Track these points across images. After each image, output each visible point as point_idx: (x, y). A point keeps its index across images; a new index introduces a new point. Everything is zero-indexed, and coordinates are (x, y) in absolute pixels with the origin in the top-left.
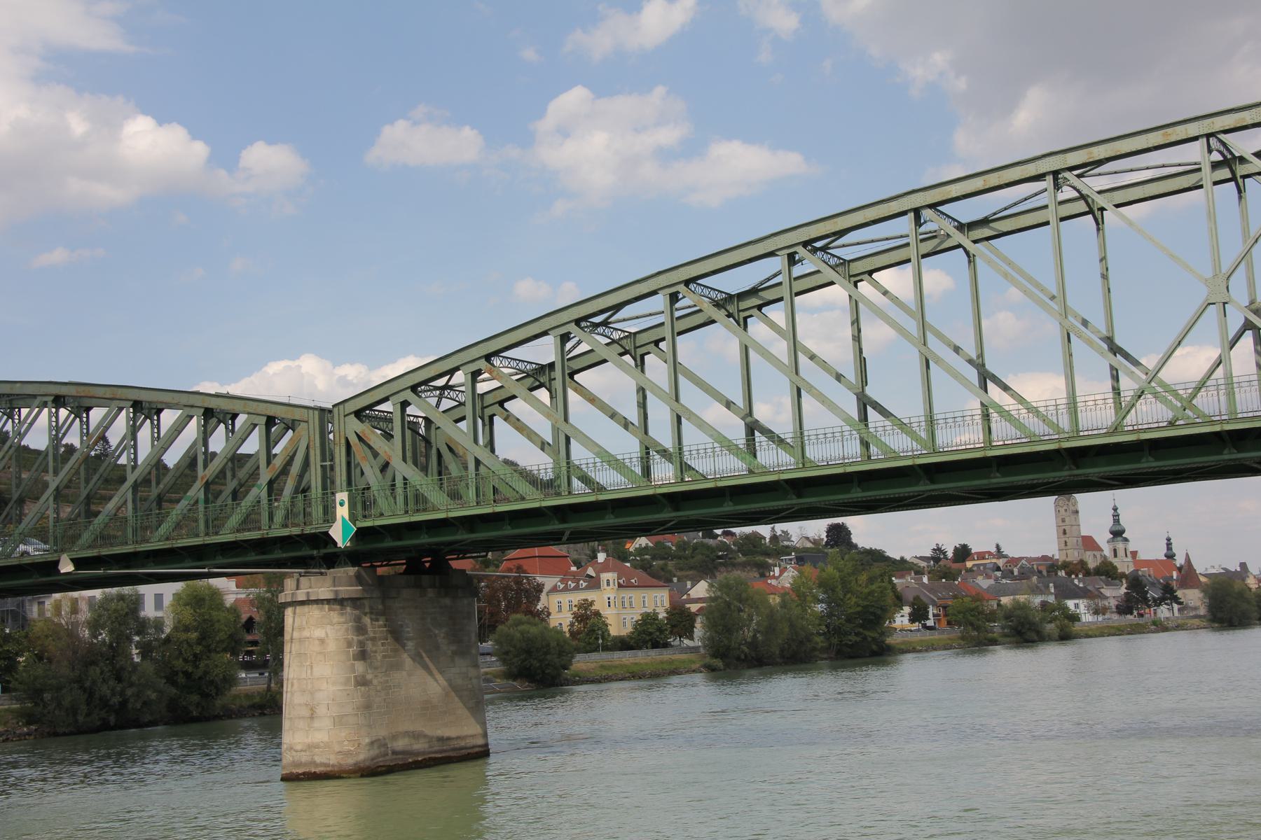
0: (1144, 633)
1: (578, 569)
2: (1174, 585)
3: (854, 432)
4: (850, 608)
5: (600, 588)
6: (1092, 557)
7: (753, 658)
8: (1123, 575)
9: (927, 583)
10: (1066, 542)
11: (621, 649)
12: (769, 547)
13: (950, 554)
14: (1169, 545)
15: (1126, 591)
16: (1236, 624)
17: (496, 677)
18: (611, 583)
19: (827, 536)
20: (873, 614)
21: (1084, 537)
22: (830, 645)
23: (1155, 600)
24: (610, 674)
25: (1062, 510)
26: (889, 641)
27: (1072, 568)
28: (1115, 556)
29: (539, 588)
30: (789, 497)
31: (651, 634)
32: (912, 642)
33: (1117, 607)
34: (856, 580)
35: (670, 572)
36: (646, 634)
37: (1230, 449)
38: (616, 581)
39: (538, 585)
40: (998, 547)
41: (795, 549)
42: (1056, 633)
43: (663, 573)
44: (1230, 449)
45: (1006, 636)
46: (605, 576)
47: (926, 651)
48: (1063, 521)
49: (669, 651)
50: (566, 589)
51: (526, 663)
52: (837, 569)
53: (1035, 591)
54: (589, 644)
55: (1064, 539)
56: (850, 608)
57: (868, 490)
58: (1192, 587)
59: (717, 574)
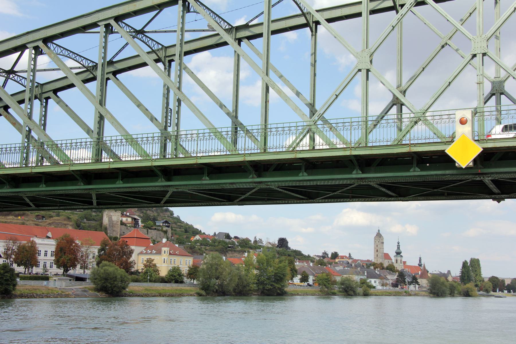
0: (400, 296)
1: (154, 244)
2: (418, 276)
3: (124, 141)
4: (269, 273)
5: (161, 254)
6: (387, 262)
7: (220, 291)
8: (398, 271)
9: (312, 266)
10: (377, 255)
11: (161, 282)
12: (252, 245)
13: (330, 256)
14: (420, 260)
15: (397, 277)
16: (440, 295)
17: (89, 290)
18: (166, 252)
19: (278, 243)
20: (279, 276)
21: (385, 254)
22: (259, 289)
23: (409, 282)
24: (149, 293)
25: (377, 242)
26: (286, 289)
27: (381, 266)
28: (397, 262)
29: (131, 252)
30: (79, 184)
31: (175, 276)
32: (298, 291)
33: (392, 283)
34: (274, 260)
35: (202, 251)
36: (173, 276)
37: (357, 171)
38: (168, 252)
39: (132, 250)
40: (350, 254)
41: (263, 247)
42: (362, 293)
43: (199, 251)
44: (357, 171)
45: (340, 292)
46: (164, 249)
47: (303, 295)
48: (377, 246)
49: (183, 285)
50: (147, 253)
51: (105, 284)
52: (265, 255)
53: (358, 274)
54: (145, 278)
55: (377, 254)
56: (269, 273)
57: (128, 183)
58: (425, 278)
59: (227, 254)
